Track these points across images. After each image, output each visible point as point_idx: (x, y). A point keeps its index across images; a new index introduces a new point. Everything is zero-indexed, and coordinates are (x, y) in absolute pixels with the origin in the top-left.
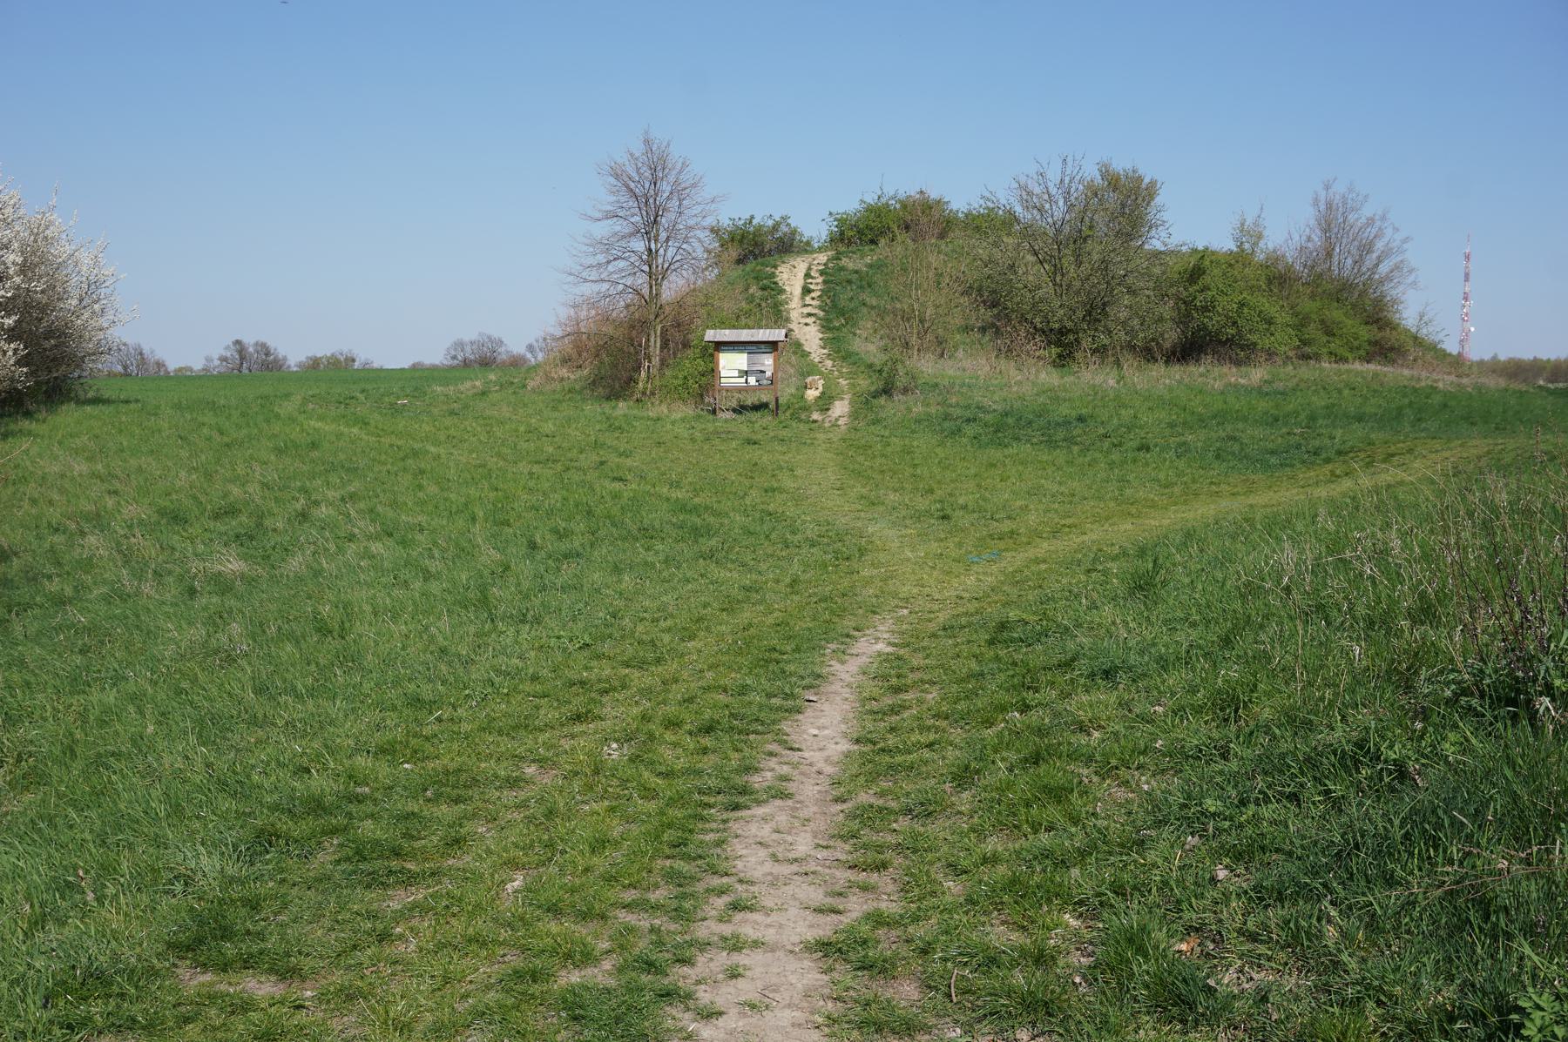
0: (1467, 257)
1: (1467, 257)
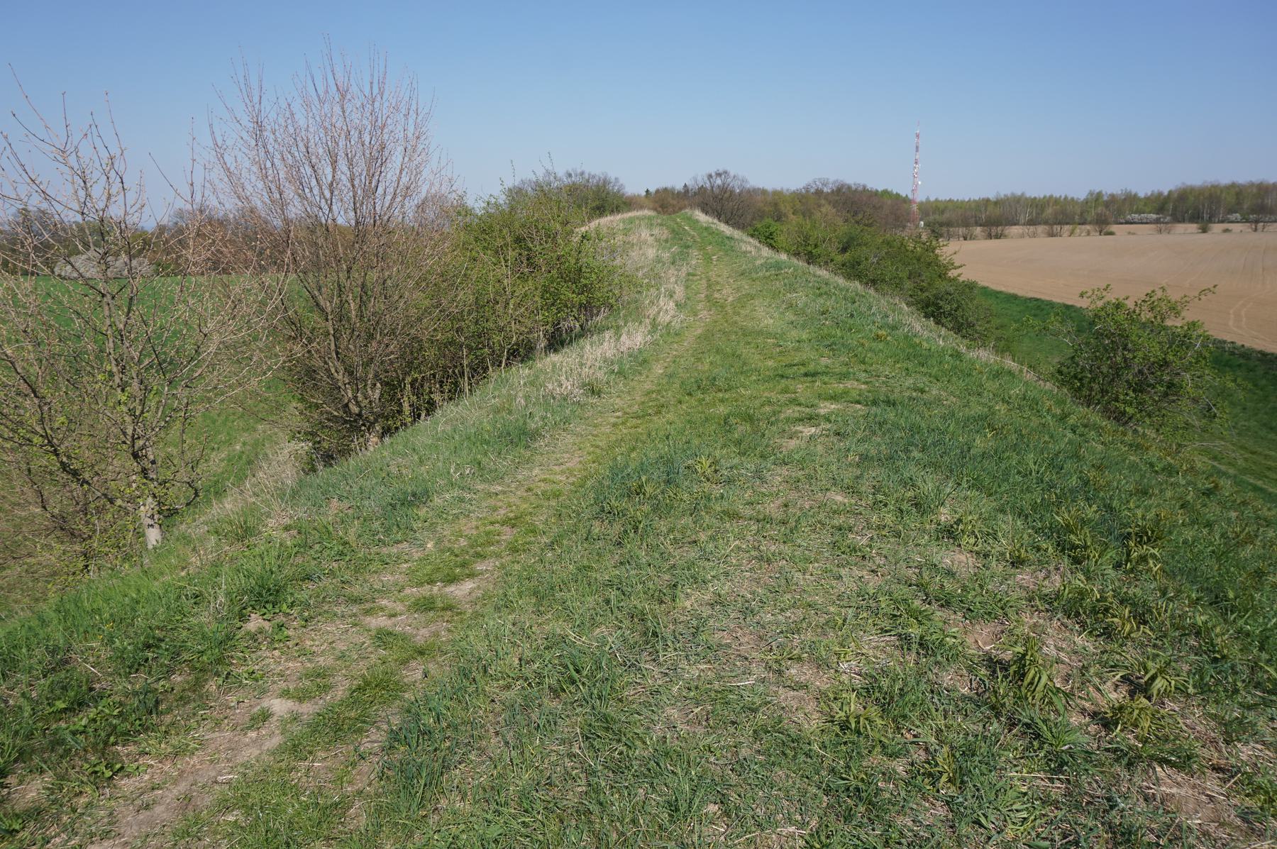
0: (918, 136)
1: (918, 136)
